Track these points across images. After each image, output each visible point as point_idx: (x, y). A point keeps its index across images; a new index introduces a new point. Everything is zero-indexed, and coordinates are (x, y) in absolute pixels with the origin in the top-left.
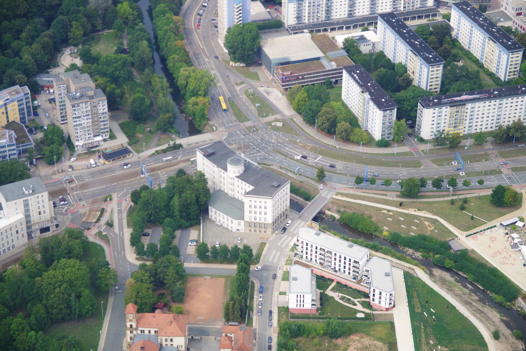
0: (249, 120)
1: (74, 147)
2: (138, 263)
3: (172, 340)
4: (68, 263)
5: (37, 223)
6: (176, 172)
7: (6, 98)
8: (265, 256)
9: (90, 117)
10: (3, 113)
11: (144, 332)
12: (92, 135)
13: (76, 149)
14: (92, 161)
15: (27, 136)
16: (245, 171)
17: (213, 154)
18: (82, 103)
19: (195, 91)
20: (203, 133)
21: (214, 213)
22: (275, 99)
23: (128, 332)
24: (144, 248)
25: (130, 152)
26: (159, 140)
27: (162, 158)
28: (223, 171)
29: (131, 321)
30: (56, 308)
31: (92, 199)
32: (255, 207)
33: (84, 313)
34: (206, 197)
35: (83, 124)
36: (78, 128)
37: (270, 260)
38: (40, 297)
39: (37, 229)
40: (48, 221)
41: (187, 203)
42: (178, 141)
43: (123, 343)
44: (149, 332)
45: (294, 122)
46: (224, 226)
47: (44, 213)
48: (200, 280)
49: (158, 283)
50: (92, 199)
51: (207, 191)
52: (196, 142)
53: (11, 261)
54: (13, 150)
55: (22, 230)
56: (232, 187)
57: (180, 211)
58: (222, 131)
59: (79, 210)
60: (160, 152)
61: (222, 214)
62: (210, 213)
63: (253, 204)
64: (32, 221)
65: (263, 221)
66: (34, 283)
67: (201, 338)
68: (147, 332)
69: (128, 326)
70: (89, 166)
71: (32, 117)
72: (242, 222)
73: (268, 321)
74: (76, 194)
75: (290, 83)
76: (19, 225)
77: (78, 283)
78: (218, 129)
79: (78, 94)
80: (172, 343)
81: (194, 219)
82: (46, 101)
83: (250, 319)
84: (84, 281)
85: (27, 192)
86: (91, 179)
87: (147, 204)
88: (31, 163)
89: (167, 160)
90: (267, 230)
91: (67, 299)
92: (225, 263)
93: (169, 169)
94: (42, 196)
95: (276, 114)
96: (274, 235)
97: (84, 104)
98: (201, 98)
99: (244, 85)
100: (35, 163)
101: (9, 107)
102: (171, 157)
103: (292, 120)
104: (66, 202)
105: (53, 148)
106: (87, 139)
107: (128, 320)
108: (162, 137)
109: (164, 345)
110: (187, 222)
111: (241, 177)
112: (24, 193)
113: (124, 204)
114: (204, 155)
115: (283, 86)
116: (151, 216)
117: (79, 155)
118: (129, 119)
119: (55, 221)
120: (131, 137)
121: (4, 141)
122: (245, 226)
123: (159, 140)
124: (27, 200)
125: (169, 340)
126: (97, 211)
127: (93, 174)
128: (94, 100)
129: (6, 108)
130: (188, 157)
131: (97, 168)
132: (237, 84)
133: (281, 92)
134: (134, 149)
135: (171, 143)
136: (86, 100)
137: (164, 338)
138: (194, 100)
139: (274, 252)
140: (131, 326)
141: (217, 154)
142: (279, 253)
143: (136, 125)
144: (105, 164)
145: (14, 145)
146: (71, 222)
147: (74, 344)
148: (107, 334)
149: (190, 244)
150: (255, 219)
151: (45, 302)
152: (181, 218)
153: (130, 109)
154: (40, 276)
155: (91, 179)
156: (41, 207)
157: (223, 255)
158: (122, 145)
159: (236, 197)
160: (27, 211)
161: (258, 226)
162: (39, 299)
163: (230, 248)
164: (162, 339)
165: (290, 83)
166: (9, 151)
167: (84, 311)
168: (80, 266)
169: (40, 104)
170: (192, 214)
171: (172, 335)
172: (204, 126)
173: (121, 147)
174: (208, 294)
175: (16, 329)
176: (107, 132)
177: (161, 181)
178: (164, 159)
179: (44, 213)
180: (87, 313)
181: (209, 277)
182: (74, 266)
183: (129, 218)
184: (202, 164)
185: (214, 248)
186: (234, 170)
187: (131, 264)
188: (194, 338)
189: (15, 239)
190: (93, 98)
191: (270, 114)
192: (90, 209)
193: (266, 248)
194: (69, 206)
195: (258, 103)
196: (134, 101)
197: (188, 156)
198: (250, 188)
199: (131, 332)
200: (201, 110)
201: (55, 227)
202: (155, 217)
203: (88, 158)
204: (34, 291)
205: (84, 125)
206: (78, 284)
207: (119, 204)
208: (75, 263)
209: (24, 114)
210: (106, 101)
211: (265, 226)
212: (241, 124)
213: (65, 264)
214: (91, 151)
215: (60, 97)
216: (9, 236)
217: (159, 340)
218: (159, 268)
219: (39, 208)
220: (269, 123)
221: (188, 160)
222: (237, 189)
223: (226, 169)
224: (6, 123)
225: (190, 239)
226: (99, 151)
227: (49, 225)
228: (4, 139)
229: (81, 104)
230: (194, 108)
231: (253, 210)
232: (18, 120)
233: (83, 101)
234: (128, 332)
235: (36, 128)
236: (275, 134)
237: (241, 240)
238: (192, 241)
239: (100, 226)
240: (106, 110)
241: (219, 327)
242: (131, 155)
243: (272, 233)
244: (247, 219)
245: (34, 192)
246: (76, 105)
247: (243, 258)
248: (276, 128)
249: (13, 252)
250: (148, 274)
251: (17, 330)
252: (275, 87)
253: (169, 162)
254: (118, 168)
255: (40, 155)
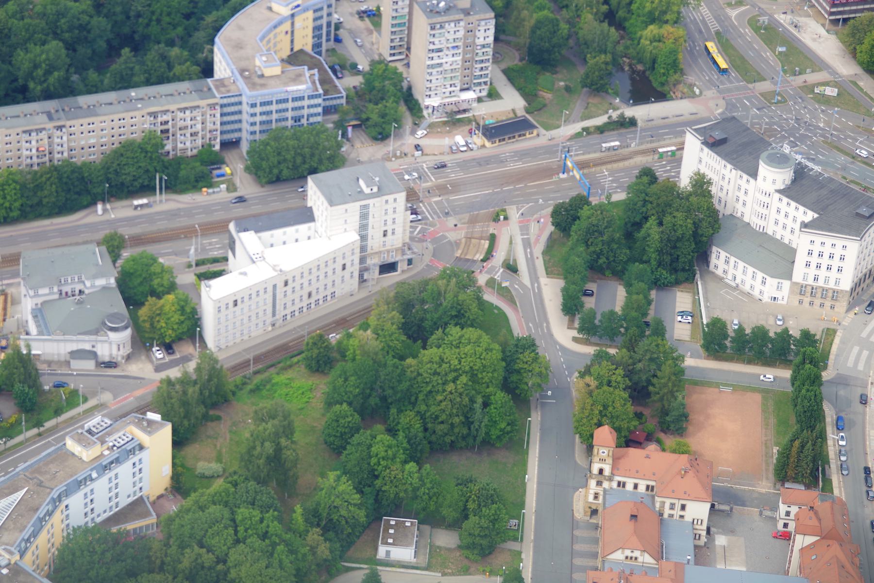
0: (765, 80)
1: (420, 110)
2: (590, 350)
3: (683, 507)
4: (467, 336)
5: (376, 253)
6: (636, 172)
7: (295, 4)
8: (837, 355)
9: (460, 51)
10: (287, 32)
11: (624, 486)
12: (458, 88)
13: (425, 113)
14: (460, 140)
15: (333, 81)
16: (794, 181)
17: (723, 141)
18: (449, 22)
19: (657, 14)
20: (672, 99)
21: (720, 260)
22: (814, 40)
23: (593, 483)
24: (595, 318)
25: (533, 127)
26: (587, 108)
27: (600, 144)
28: (745, 177)
29: (602, 460)
30: (442, 422)
31: (468, 215)
32: (831, 257)
33: (494, 437)
34: (713, 227)
35: (445, 65)
36: (434, 71)
37: (850, 363)
38: (413, 398)
39: (374, 265)
40: (397, 250)
41: (654, 240)
42: (630, 112)
43: (572, 502)
44: (636, 486)
45: (861, 90)
46: (742, 287)
47: (393, 233)
48: (710, 393)
49: (639, 393)
50: (468, 215)
51: (713, 215)
52: (664, 115)
53: (331, 324)
54: (316, 106)
55: (352, 264)
56: (764, 211)
57: (660, 252)
58: (713, 98)
59: (447, 234)
60: (592, 130)
61: (741, 264)
62: (713, 260)
63: (816, 248)
64: (369, 249)
65: (831, 285)
66: (404, 372)
67: (731, 509)
68: (629, 487)
69: (595, 470)
70: (454, 148)
71: (332, 43)
72: (786, 284)
73: (865, 489)
74: (436, 202)
75: (847, 8)
76: (348, 254)
77: (486, 377)
78: (704, 93)
79: (442, 4)
80: (682, 513)
81: (683, 270)
82: (351, 14)
83: (828, 482)
84: (496, 375)
85: (367, 191)
86: (461, 175)
87: (593, 231)
88: (344, 135)
89: (609, 149)
90: (837, 304)
91: (465, 406)
92: (757, 364)
93: (615, 166)
94: (395, 200)
95: (820, 70)
96: (851, 315)
97: (452, 25)
98: (667, 29)
99: (743, 8)
100: (350, 135)
101: (299, 22)
102: (617, 143)
103: (855, 84)
104: (420, 217)
105: (386, 106)
106: (447, 94)
107: (596, 459)
108: (590, 101)
109: (666, 516)
110: (671, 274)
111: (787, 192)
112: (361, 192)
113: (534, 228)
114: (705, 143)
115: (832, 14)
116: (599, 258)
117: (431, 126)
118: (521, 60)
119: (408, 252)
120: (529, 96)
121: (302, 87)
122: (792, 292)
123: (587, 108)
124: (366, 207)
125: (678, 507)
126: (481, 238)
127: (464, 165)
128: (471, 19)
129: (293, 24)
130: (650, 146)
131: (470, 154)
132: (729, 5)
133: (823, 25)
134: (537, 121)
135: (615, 115)
136: (457, 17)
137: (668, 502)
138: (655, 32)
139: (856, 349)
140: (601, 471)
141: (734, 142)
142: (865, 353)
143: (538, 73)
144: (483, 146)
145: (319, 96)
146: (434, 255)
147: (492, 496)
148: (539, 483)
149: (679, 318)
150: (816, 279)
151: (423, 408)
152: (659, 266)
153: (528, 41)
154: (415, 357)
155: (461, 175)
156: (389, 222)
157: (760, 346)
158: (513, 111)
159: (770, 232)
160: (363, 228)
161: (819, 295)
162: (410, 403)
163: (772, 334)
164: (665, 504)
165: (847, 8)
166: (309, 107)
167: (495, 433)
168: (489, 344)
169: (342, 20)
170: (681, 260)
171: (686, 496)
172: (675, 85)
173: (512, 115)
174: (734, 423)
175: (383, 454)
176: (485, 83)
177: (613, 190)
178: (604, 145)
179: (393, 233)
180: (499, 437)
181: (729, 390)
182: (477, 343)
183: (547, 258)
184: (697, 160)
185: (741, 330)
186: (773, 175)
187: (563, 349)
188: (717, 507)
189: (338, 281)
190: (469, 14)
191: (808, 70)
192: (467, 233)
193: (837, 341)
194: (426, 224)
195: (781, 46)
196: (539, 25)
197: (651, 142)
198: (810, 215)
199: (599, 483)
200: (670, 53)
201: (406, 263)
202: (607, 259)
203: (449, 132)
204: (405, 385)
205: (447, 67)
206: (486, 380)
207: (524, 229)
208: (480, 337)
209: (319, 37)
210: (493, 22)
211: (836, 294)
212: (750, 86)
213: (461, 337)
214: (455, 119)
215: (395, 7)
216: (330, 273)
217: (658, 505)
218: (640, 361)
219: (385, 224)
220: (809, 88)
221: (654, 151)
222: (773, 215)
223: (754, 174)
224: (288, 53)
225: (678, 310)
226: (469, 121)
227: (397, 259)
228: (301, 83)
229: (447, 24)
230: (655, 48)
231: (814, 260)
232: (309, 49)
233: (452, 18)
234: (593, 483)
235: (343, 67)
236: (823, 111)
237: (783, 319)
238: (682, 313)
239: (493, 269)
240: (491, 39)
241: (764, 491)
242: (535, 132)
243: (848, 311)
244: (797, 277)
245: (381, 192)
246: (438, 26)
247: (800, 354)
248: (824, 100)
249: (332, 306)
250: (620, 371)
251: (383, 459)
252: (809, 16)
253: (614, 153)
254: (512, 157)
255: (356, 119)
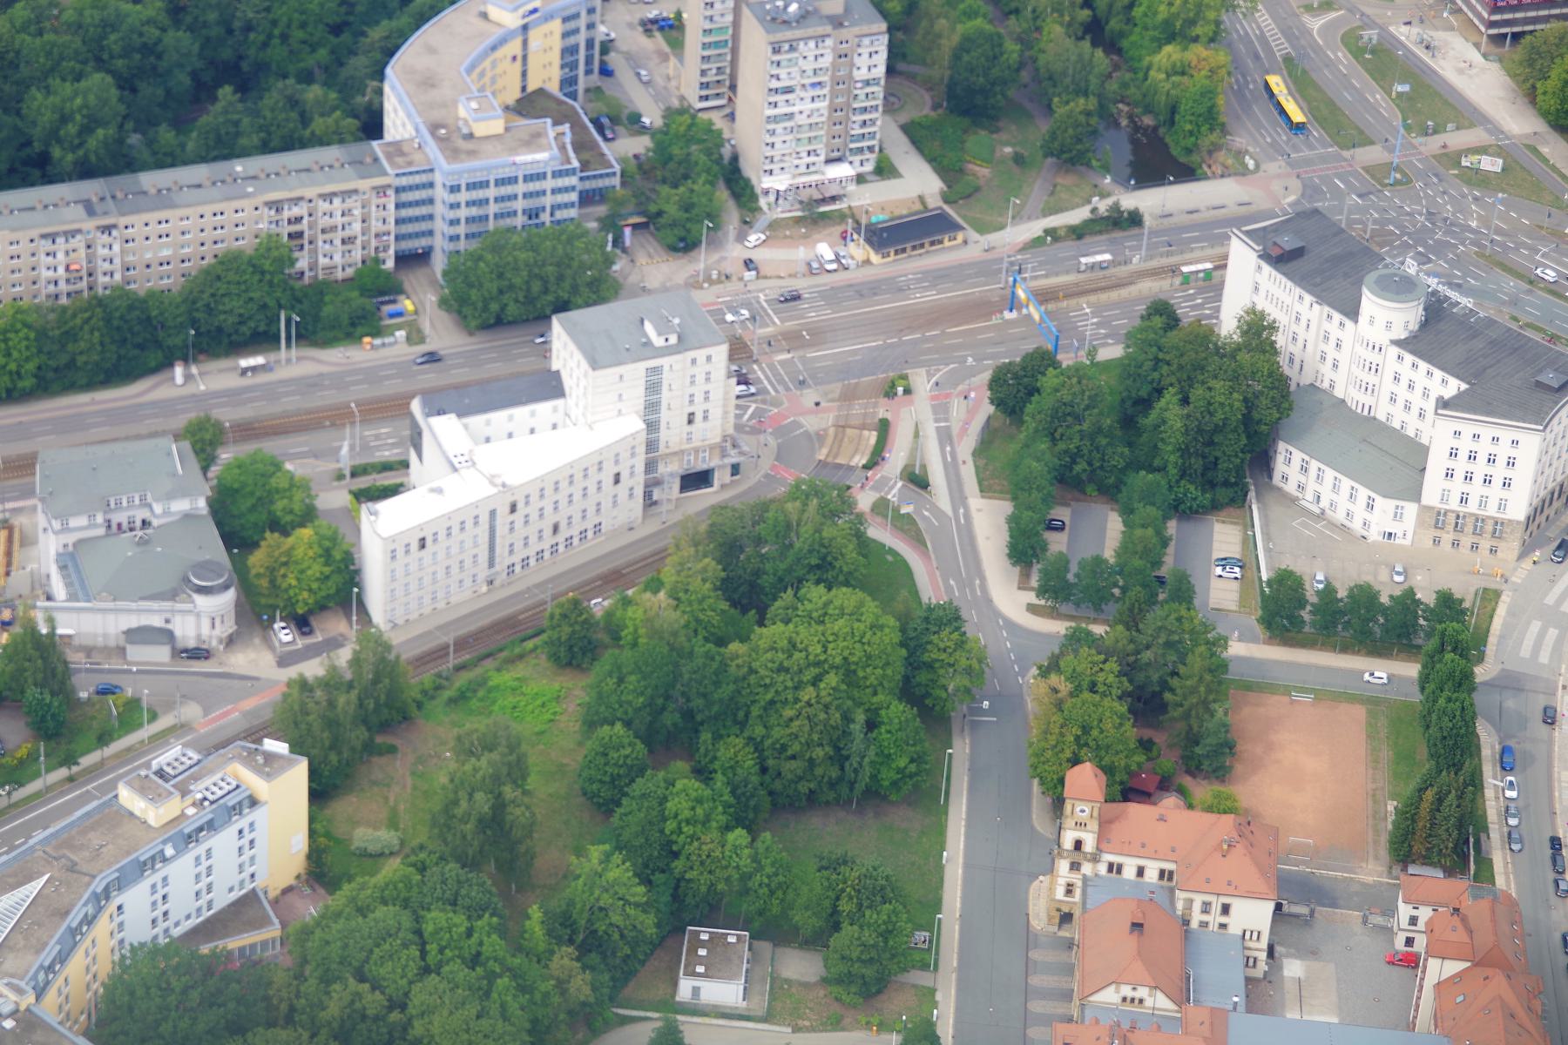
0: (1372, 143)
1: (754, 197)
2: (1059, 627)
3: (1226, 909)
4: (837, 603)
5: (675, 453)
6: (1141, 308)
7: (530, 7)
8: (1502, 637)
9: (826, 91)
10: (514, 58)
11: (1119, 871)
12: (822, 158)
13: (763, 202)
14: (825, 250)
15: (597, 145)
16: (1425, 325)
17: (1297, 253)
18: (806, 39)
19: (1178, 24)
20: (1205, 177)
21: (1292, 465)
22: (1461, 72)
23: (1063, 866)
24: (1067, 570)
25: (957, 227)
26: (1052, 193)
27: (1076, 258)
28: (1337, 316)
29: (1080, 825)
30: (793, 757)
31: (839, 385)
32: (1491, 460)
33: (886, 783)
34: (1278, 408)
35: (798, 117)
36: (779, 127)
37: (1526, 651)
38: (741, 714)
39: (672, 475)
40: (712, 448)
41: (1174, 431)
42: (1131, 200)
43: (1027, 900)
44: (1141, 872)
45: (1545, 161)
46: (1330, 515)
47: (705, 418)
48: (1274, 704)
49: (1147, 704)
50: (839, 385)
51: (1279, 385)
52: (1191, 207)
53: (593, 581)
54: (566, 190)
55: (632, 474)
56: (1371, 379)
57: (1184, 451)
58: (1279, 176)
59: (801, 419)
60: (1062, 233)
61: (1330, 474)
62: (1280, 466)
63: (1465, 445)
64: (662, 446)
65: (1492, 511)
66: (724, 666)
67: (1312, 912)
68: (1129, 873)
69: (1068, 843)
70: (815, 265)
71: (595, 78)
72: (1411, 509)
73: (1551, 876)
74: (782, 363)
75: (1519, 15)
76: (624, 455)
77: (872, 675)
78: (1263, 167)
79: (793, 8)
80: (1224, 920)
81: (1226, 484)
82: (630, 25)
83: (1485, 865)
84: (889, 672)
85: (658, 342)
86: (827, 314)
87: (1064, 415)
88: (618, 242)
89: (1092, 267)
90: (1502, 545)
91: (835, 728)
92: (1358, 653)
93: (1104, 297)
94: (709, 358)
95: (1472, 125)
96: (1527, 564)
97: (812, 44)
98: (1197, 51)
99: (1334, 15)
100: (628, 242)
101: (536, 39)
102: (1107, 257)
103: (1534, 150)
104: (753, 390)
105: (692, 191)
106: (803, 169)
107: (1069, 823)
108: (1059, 180)
109: (1194, 924)
110: (1204, 491)
111: (1411, 344)
112: (648, 344)
113: (957, 409)
114: (1265, 256)
115: (1492, 24)
116: (1074, 462)
117: (774, 226)
118: (935, 107)
119: (733, 452)
120: (949, 171)
121: (542, 156)
122: (1420, 523)
123: (1052, 193)
124: (656, 370)
125: (1216, 908)
126: (863, 427)
127: (832, 296)
128: (845, 33)
129: (525, 43)
130: (1165, 261)
131: (842, 275)
132: (1309, 8)
133: (1477, 46)
134: (964, 217)
135: (1103, 206)
136: (820, 30)
137: (1198, 900)
138: (1175, 57)
139: (1536, 626)
140: (1078, 845)
141: (1317, 255)
142: (1553, 633)
143: (965, 131)
144: (867, 262)
145: (573, 172)
146: (778, 458)
147: (883, 888)
148: (967, 866)
149: (1219, 570)
150: (1464, 500)
151: (759, 731)
152: (1182, 477)
153: (948, 73)
154: (744, 639)
155: (827, 314)
156: (699, 398)
157: (1364, 621)
158: (921, 198)
159: (1382, 417)
160: (652, 408)
161: (1469, 529)
162: (736, 722)
163: (1384, 599)
164: (1192, 903)
165: (1519, 15)
166: (554, 192)
167: (887, 776)
168: (877, 617)
169: (613, 35)
170: (1223, 465)
171: (1231, 890)
172: (1210, 153)
173: (918, 207)
174: (1317, 758)
175: (687, 814)
176: (871, 149)
177: (1099, 340)
178: (1083, 260)
179: (705, 418)
180: (894, 784)
181: (1307, 698)
182: (856, 614)
183: (982, 463)
184: (1251, 287)
185: (1329, 591)
186: (1387, 314)
187: (1011, 625)
188: (1286, 909)
189: (607, 504)
190: (841, 25)
191: (1450, 126)
192: (838, 417)
193: (1501, 611)
194: (764, 402)
195: (1402, 82)
196: (967, 44)
197: (1168, 254)
198: (1454, 386)
199: (1075, 866)
200: (1202, 95)
201: (729, 471)
202: (1090, 464)
203: (805, 237)
204: (726, 691)
205: (802, 120)
206: (872, 680)
207: (941, 411)
208: (861, 604)
209: (573, 66)
210: (885, 39)
211: (1499, 528)
212: (1346, 154)
213: (826, 605)
214: (816, 213)
215: (708, 13)
216: (592, 489)
217: (1180, 906)
218: (1148, 647)
219: (691, 402)
220: (1451, 158)
221: (1174, 270)
222: (1388, 386)
223: (1352, 312)
224: (517, 94)
225: (1216, 555)
226: (841, 217)
227: (712, 465)
228: (541, 149)
229: (802, 44)
230: (1175, 85)
231: (1461, 466)
232: (554, 87)
233: (810, 32)
234: (1063, 866)
235: (615, 120)
236: (1476, 199)
237: (1405, 573)
238: (1224, 562)
239: (884, 481)
240: (880, 71)
241: (1370, 879)
242: (960, 237)
243: (1521, 557)
244: (1431, 496)
245: (683, 345)
246: (786, 47)
247: (1435, 635)
248: (1478, 178)
249: (595, 548)
250: (1113, 665)
251: (688, 822)
252: (1452, 29)
253: (1101, 274)
254: (919, 281)
255: (639, 214)
